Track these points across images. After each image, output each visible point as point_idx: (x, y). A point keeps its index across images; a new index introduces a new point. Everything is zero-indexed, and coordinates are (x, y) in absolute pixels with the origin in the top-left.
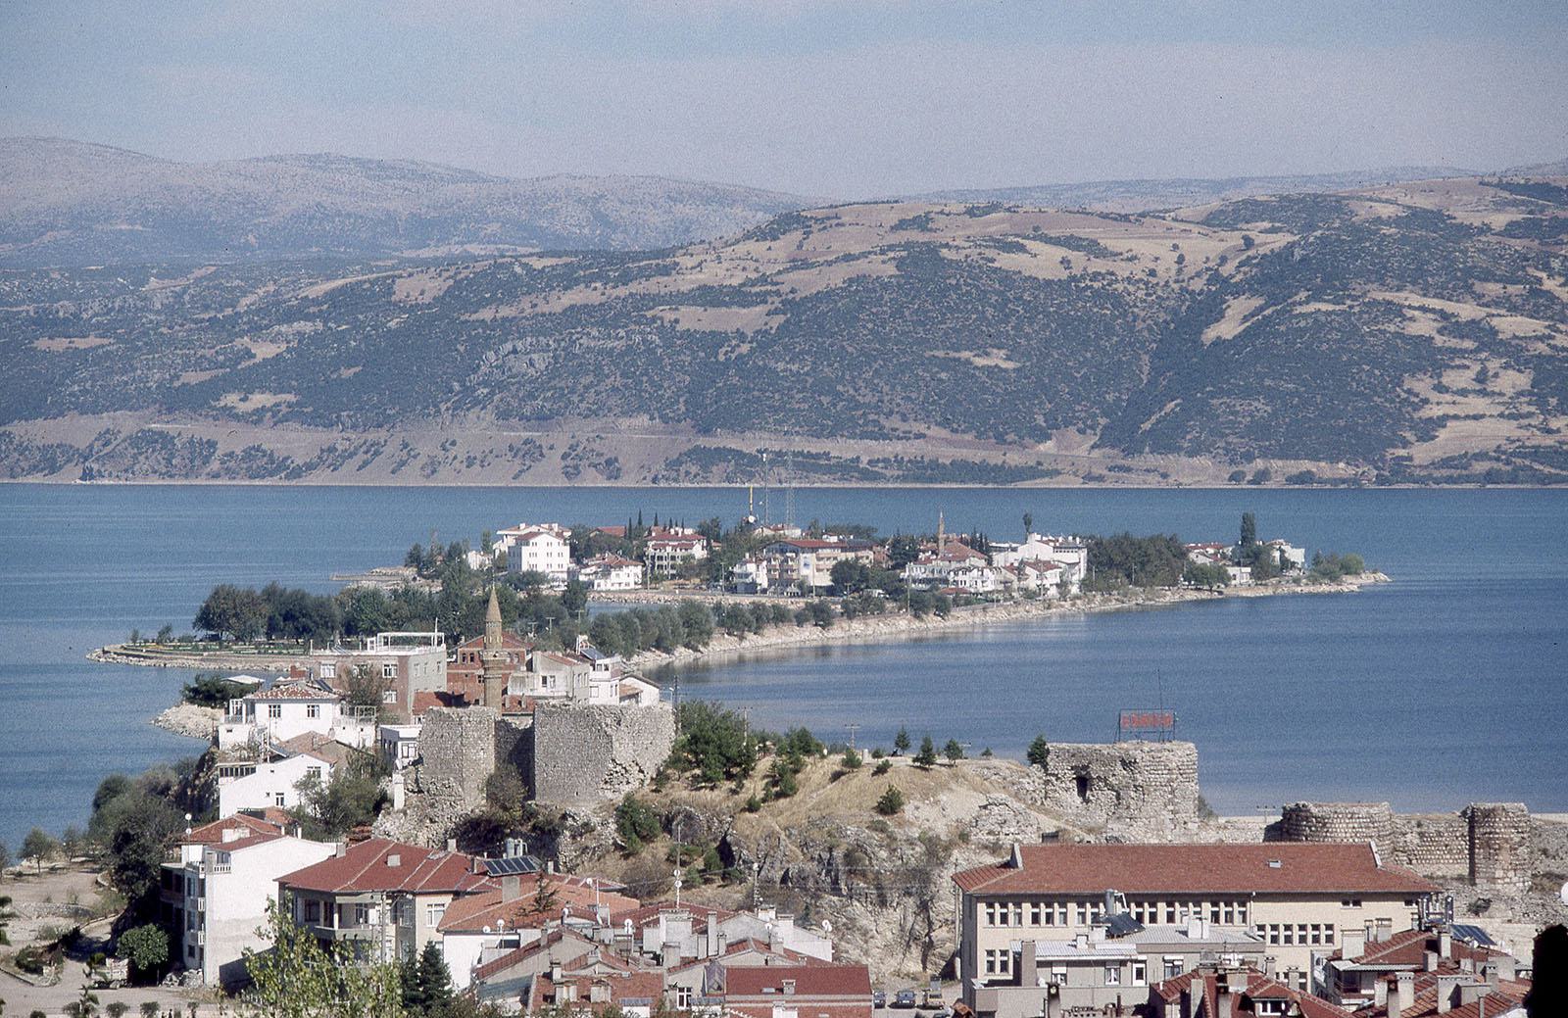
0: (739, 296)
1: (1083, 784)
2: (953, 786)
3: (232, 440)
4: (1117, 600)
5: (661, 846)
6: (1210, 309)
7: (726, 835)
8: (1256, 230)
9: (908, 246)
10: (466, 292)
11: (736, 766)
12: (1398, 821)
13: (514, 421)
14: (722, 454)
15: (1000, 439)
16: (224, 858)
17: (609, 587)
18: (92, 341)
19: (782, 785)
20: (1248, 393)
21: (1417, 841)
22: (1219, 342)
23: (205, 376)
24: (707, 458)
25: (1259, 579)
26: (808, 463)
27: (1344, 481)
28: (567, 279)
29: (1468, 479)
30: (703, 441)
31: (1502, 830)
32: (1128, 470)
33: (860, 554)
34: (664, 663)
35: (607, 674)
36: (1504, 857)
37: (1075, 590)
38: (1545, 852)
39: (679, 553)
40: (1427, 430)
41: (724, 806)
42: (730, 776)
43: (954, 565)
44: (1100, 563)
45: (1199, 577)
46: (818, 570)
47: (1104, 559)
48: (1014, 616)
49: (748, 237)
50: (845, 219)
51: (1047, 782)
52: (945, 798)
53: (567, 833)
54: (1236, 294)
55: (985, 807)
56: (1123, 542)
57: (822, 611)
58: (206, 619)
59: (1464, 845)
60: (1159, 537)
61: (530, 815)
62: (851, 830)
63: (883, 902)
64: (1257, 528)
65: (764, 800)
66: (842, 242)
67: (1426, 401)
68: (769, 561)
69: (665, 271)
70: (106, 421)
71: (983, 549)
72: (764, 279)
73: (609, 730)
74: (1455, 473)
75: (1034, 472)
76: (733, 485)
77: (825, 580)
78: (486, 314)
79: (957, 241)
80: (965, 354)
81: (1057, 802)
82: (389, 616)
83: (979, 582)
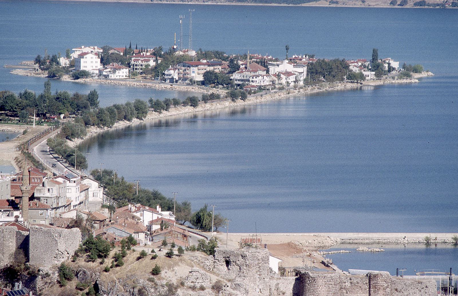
1: (228, 263)
2: (180, 264)
4: (318, 88)
7: (97, 281)
11: (102, 254)
12: (343, 278)
17: (115, 77)
19: (118, 261)
21: (349, 285)
25: (378, 77)
27: (438, 5)
31: (380, 282)
33: (215, 67)
34: (127, 125)
35: (75, 184)
37: (301, 83)
38: (396, 290)
39: (144, 63)
41: (97, 269)
43: (252, 74)
44: (312, 72)
45: (352, 77)
46: (198, 74)
47: (314, 71)
48: (273, 98)
51: (215, 262)
52: (176, 269)
53: (40, 277)
55: (191, 272)
56: (321, 63)
57: (194, 100)
59: (367, 287)
60: (338, 60)
61: (27, 268)
62: (141, 281)
64: (379, 54)
65: (111, 267)
68: (179, 70)
71: (264, 64)
73: (56, 239)
76: (184, 3)
81: (218, 269)
82: (18, 105)
83: (262, 81)
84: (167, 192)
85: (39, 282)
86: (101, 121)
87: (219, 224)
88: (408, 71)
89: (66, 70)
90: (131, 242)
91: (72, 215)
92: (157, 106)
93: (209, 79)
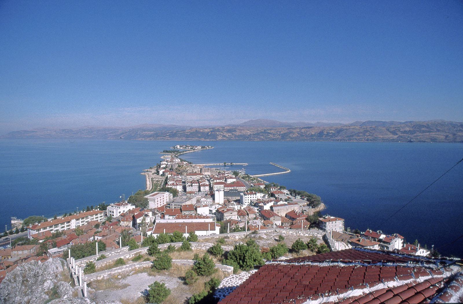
3: (166, 138)
5: (177, 170)
11: (180, 167)
45: (206, 148)
58: (163, 151)
84: (187, 160)
85: (174, 170)
86: (180, 153)
87: (192, 163)
88: (211, 147)
89: (176, 148)
90: (183, 165)
91: (177, 163)
92: (186, 151)
93: (191, 148)
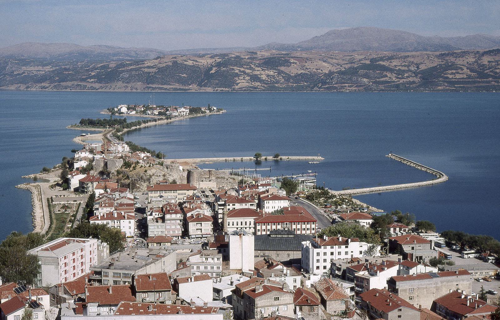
0: (152, 67)
1: (167, 168)
3: (89, 85)
6: (211, 69)
8: (216, 58)
9: (173, 61)
10: (118, 67)
13: (124, 83)
14: (150, 87)
15: (185, 85)
16: (73, 177)
18: (71, 72)
19: (134, 168)
20: (215, 80)
22: (212, 73)
23: (86, 77)
24: (149, 88)
26: (161, 89)
27: (227, 91)
28: (131, 65)
29: (242, 90)
30: (148, 86)
31: (212, 172)
32: (201, 89)
36: (213, 175)
37: (187, 114)
40: (237, 84)
42: (129, 167)
49: (153, 59)
50: (166, 57)
54: (214, 67)
58: (80, 123)
62: (141, 174)
63: (145, 182)
66: (165, 60)
67: (237, 81)
69: (143, 64)
70: (73, 83)
71: (176, 109)
72: (155, 65)
74: (241, 90)
75: (189, 90)
77: (157, 114)
78: (121, 69)
79: (179, 60)
80: (180, 75)
